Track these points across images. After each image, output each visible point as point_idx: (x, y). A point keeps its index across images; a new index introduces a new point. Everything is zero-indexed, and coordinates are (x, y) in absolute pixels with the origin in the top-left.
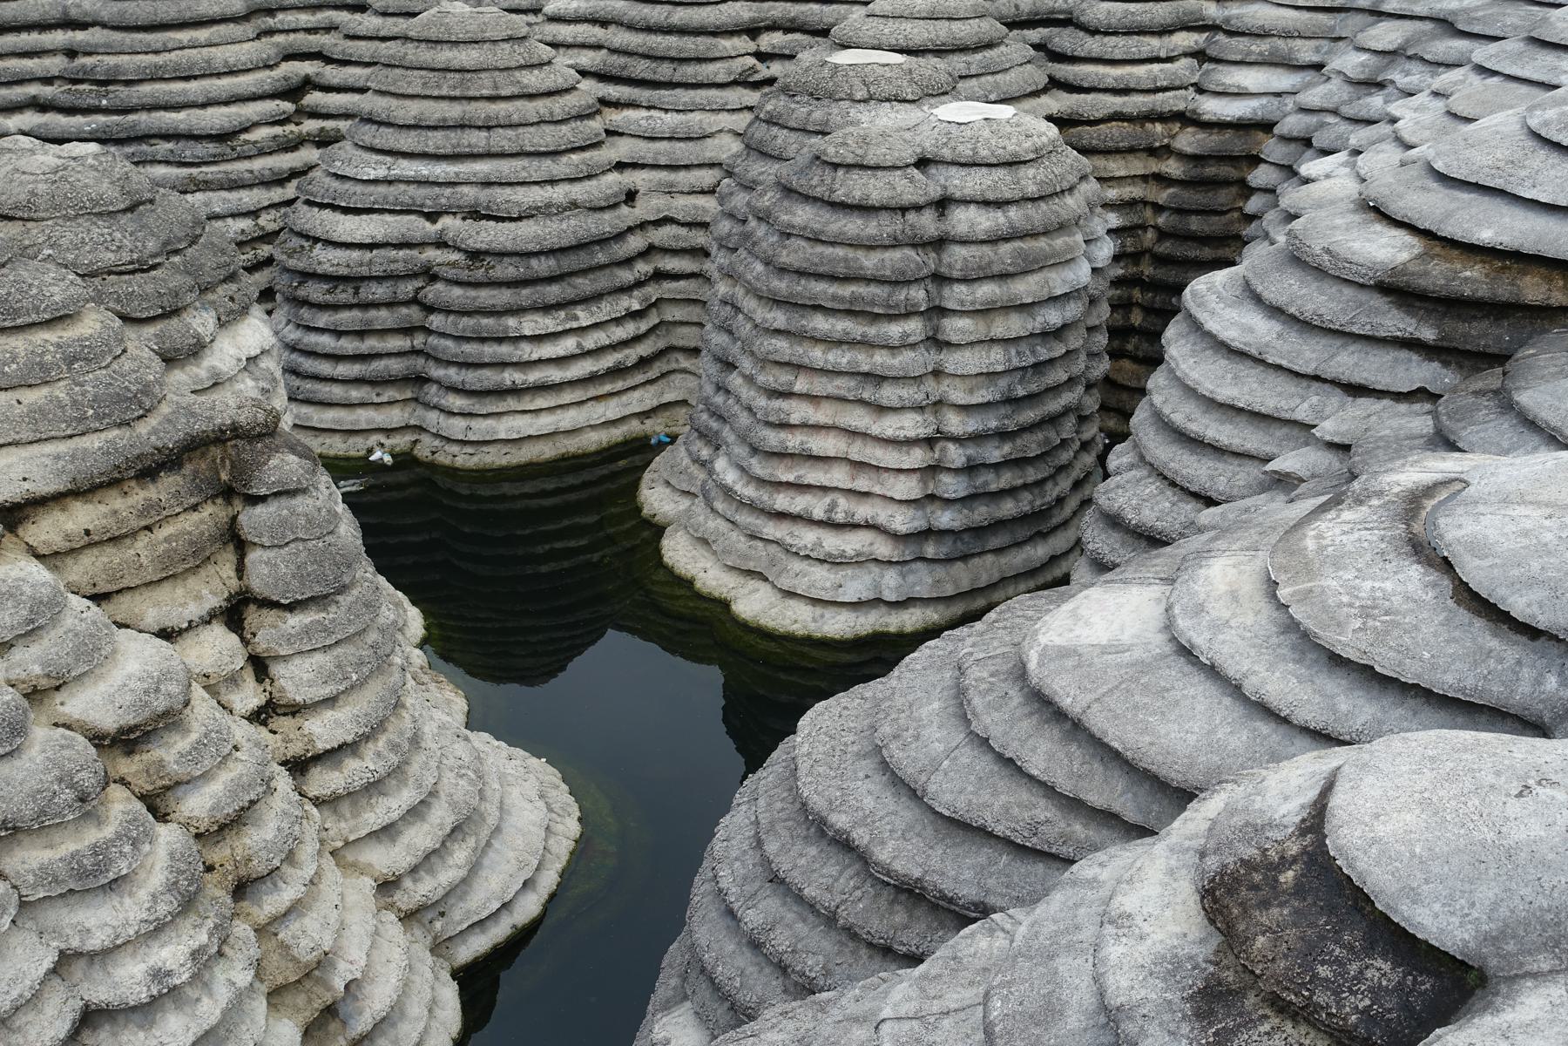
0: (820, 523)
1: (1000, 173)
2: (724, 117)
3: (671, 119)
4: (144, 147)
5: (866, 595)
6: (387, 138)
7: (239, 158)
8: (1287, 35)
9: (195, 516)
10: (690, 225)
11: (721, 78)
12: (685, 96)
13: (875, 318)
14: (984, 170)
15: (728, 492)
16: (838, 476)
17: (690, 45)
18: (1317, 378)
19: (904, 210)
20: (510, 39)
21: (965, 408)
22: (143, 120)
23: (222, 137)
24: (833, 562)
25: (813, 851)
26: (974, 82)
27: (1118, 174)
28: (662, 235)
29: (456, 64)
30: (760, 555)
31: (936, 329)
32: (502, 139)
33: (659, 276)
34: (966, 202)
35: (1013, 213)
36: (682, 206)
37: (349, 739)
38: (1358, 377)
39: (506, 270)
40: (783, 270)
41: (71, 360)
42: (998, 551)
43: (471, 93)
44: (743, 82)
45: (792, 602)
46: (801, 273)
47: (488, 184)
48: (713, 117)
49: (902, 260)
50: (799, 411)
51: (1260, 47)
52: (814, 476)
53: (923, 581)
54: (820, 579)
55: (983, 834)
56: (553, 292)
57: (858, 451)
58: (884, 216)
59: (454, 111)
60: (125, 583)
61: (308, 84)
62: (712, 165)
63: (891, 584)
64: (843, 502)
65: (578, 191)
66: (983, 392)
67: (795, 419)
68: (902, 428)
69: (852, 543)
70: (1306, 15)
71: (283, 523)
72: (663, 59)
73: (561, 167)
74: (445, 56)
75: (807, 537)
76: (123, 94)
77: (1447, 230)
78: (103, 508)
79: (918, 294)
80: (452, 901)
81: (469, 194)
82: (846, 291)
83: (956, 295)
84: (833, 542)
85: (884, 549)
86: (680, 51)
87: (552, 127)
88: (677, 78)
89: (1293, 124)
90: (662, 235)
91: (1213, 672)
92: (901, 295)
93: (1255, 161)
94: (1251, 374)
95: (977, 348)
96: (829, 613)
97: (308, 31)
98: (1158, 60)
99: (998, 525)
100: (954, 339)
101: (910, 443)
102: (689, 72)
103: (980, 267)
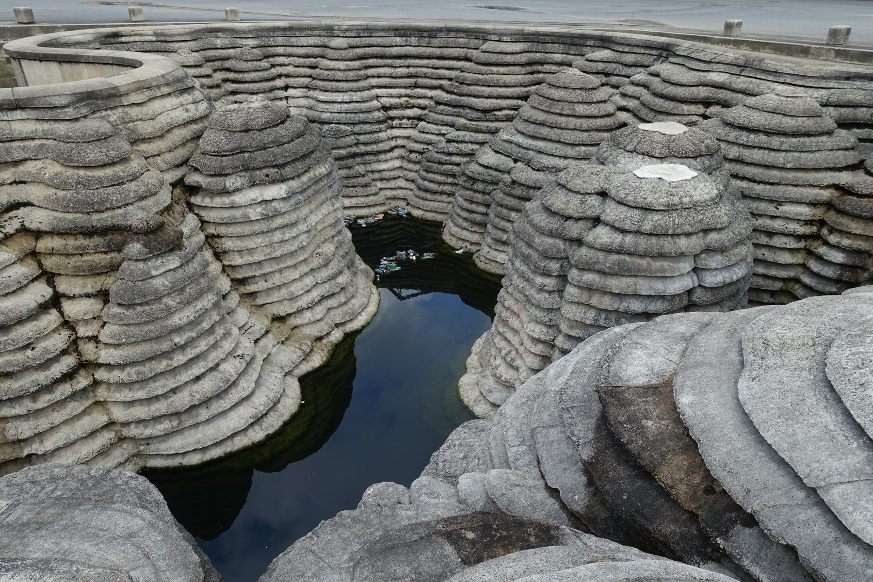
4: (461, 110)
7: (486, 121)
9: (104, 256)
14: (626, 208)
20: (581, 89)
22: (465, 100)
23: (485, 111)
26: (783, 154)
27: (854, 231)
32: (554, 134)
35: (629, 239)
37: (112, 363)
41: (78, 183)
43: (552, 110)
47: (540, 152)
49: (550, 245)
60: (60, 272)
66: (578, 331)
68: (533, 331)
76: (465, 89)
78: (64, 242)
79: (554, 266)
80: (155, 441)
86: (659, 107)
87: (580, 133)
95: (581, 306)
103: (587, 263)
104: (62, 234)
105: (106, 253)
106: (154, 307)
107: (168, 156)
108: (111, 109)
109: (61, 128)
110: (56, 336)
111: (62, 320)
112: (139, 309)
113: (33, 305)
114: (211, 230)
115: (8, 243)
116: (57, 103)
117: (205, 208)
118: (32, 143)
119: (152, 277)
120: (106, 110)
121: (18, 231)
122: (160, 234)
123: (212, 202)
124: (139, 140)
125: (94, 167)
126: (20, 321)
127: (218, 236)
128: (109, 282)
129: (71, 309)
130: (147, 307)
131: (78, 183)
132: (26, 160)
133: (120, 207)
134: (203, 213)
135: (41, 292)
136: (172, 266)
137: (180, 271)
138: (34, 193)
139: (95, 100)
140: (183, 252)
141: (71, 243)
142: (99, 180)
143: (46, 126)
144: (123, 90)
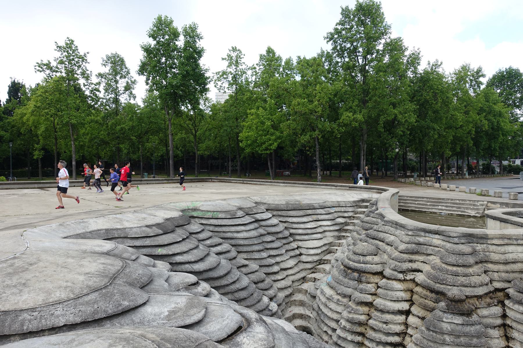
9: (432, 303)
41: (438, 269)
104: (424, 287)
105: (434, 302)
106: (438, 336)
107: (503, 275)
108: (480, 244)
109: (448, 245)
110: (399, 326)
111: (405, 321)
112: (431, 333)
113: (396, 309)
114: (508, 322)
115: (404, 283)
116: (452, 235)
117: (509, 308)
118: (437, 249)
119: (443, 321)
120: (477, 243)
121: (411, 280)
122: (459, 304)
123: (513, 306)
124: (488, 261)
125: (449, 265)
126: (388, 312)
127: (511, 327)
128: (429, 316)
129: (412, 320)
130: (434, 334)
131: (438, 269)
132: (431, 255)
133: (451, 286)
134: (508, 311)
135: (405, 306)
136: (456, 322)
137: (460, 327)
138: (426, 268)
139: (470, 238)
140: (468, 319)
141: (425, 292)
142: (447, 271)
143: (445, 243)
144: (490, 236)
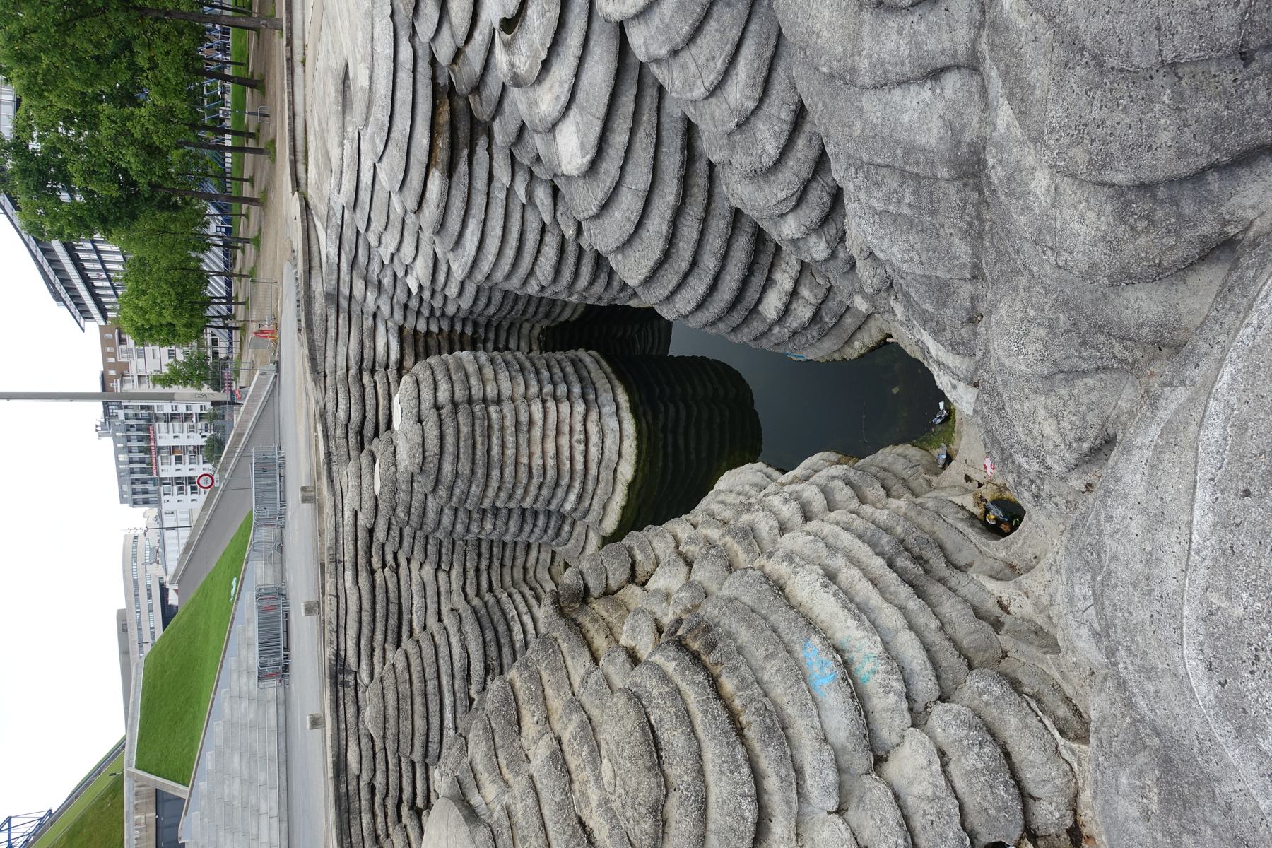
0: (587, 446)
1: (422, 387)
2: (413, 575)
3: (417, 601)
5: (615, 418)
6: (434, 736)
8: (361, 332)
10: (465, 579)
11: (395, 579)
12: (405, 594)
13: (490, 426)
15: (580, 498)
16: (564, 441)
17: (380, 597)
18: (488, 194)
19: (441, 420)
21: (527, 388)
24: (603, 437)
25: (681, 244)
28: (471, 590)
29: (395, 704)
30: (606, 475)
31: (493, 402)
32: (431, 673)
33: (490, 589)
34: (436, 397)
36: (456, 585)
38: (486, 176)
39: (493, 651)
40: (473, 472)
42: (589, 373)
44: (396, 569)
45: (623, 452)
46: (473, 463)
47: (453, 676)
48: (414, 581)
50: (537, 461)
51: (367, 343)
52: (565, 452)
53: (606, 397)
54: (611, 441)
55: (656, 158)
56: (502, 628)
57: (551, 432)
58: (444, 428)
59: (418, 700)
61: (413, 806)
62: (437, 577)
63: (609, 409)
64: (575, 438)
65: (453, 631)
67: (541, 462)
69: (593, 429)
70: (353, 327)
71: (595, 570)
72: (387, 610)
73: (441, 641)
74: (391, 712)
75: (594, 452)
77: (425, 159)
79: (477, 408)
81: (458, 683)
82: (479, 439)
83: (476, 392)
84: (594, 439)
85: (594, 415)
88: (396, 601)
89: (398, 316)
90: (471, 590)
91: (577, 76)
92: (478, 414)
93: (415, 332)
94: (490, 224)
96: (625, 433)
97: (386, 817)
98: (375, 387)
99: (577, 371)
100: (496, 392)
101: (544, 408)
102: (393, 596)
